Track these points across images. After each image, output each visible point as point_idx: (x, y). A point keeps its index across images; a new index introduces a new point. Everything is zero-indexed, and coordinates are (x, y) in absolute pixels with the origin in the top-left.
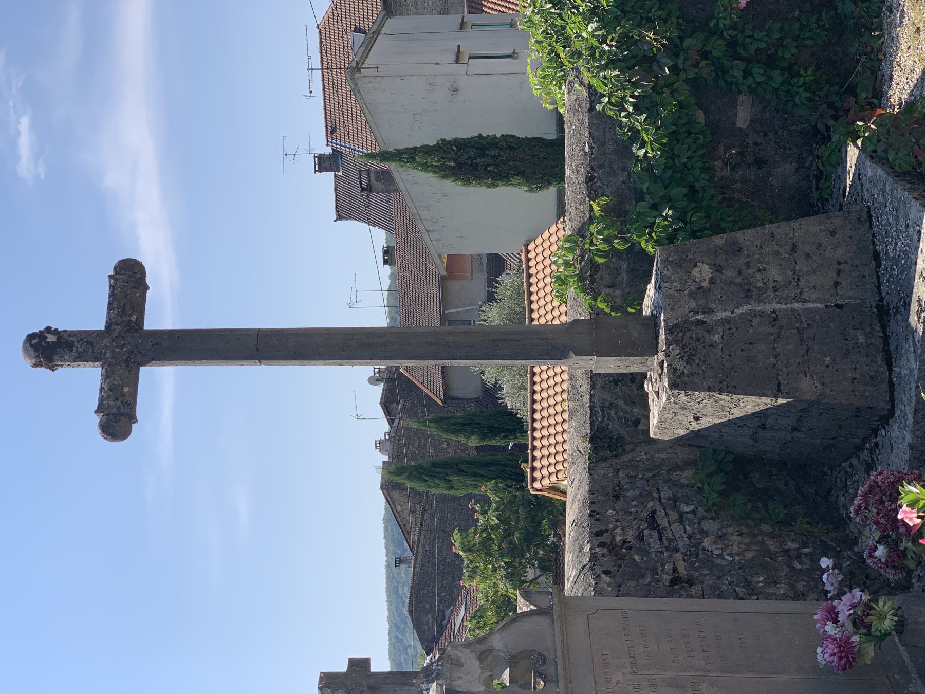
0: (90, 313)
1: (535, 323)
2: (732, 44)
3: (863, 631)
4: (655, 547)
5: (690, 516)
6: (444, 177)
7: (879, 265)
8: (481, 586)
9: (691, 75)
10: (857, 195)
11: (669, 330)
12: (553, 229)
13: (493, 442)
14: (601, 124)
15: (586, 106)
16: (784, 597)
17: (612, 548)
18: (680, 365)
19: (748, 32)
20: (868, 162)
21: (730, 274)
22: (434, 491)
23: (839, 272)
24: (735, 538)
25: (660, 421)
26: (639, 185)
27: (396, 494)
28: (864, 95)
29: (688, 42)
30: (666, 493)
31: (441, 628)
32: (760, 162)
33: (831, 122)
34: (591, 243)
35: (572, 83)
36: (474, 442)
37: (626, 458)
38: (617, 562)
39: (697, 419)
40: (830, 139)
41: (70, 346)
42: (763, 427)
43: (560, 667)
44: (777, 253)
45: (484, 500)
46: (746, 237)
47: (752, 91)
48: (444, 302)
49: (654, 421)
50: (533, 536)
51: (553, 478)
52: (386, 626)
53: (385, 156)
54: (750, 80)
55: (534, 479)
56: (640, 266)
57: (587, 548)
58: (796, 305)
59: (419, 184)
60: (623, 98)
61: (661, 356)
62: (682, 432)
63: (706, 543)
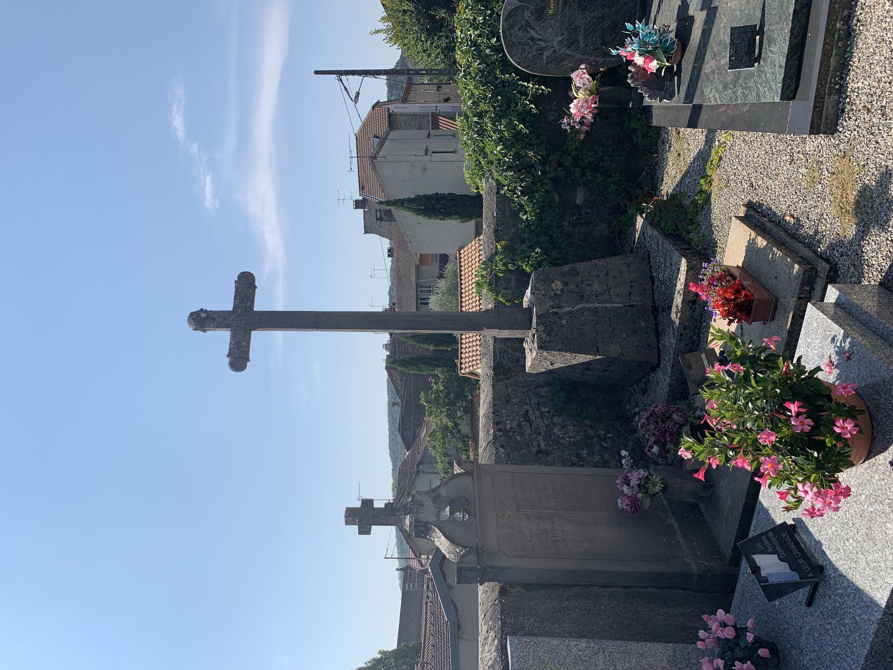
0: (225, 302)
1: (464, 309)
2: (576, 159)
3: (643, 490)
4: (528, 431)
5: (547, 414)
6: (418, 214)
7: (653, 284)
8: (434, 421)
9: (553, 176)
10: (642, 244)
11: (538, 317)
12: (473, 243)
13: (441, 348)
14: (503, 201)
15: (495, 191)
16: (596, 466)
17: (505, 432)
18: (544, 336)
19: (584, 152)
20: (649, 227)
21: (572, 287)
22: (411, 372)
23: (632, 287)
24: (571, 428)
25: (532, 364)
26: (523, 235)
27: (393, 371)
28: (646, 189)
29: (552, 157)
30: (534, 401)
31: (414, 438)
32: (588, 223)
33: (628, 203)
34: (496, 266)
35: (487, 178)
36: (431, 348)
37: (512, 380)
38: (504, 437)
39: (552, 364)
40: (627, 211)
41: (214, 319)
42: (588, 369)
43: (477, 508)
44: (598, 276)
45: (436, 377)
46: (582, 266)
47: (585, 184)
48: (418, 277)
49: (528, 364)
50: (460, 395)
51: (471, 368)
52: (388, 433)
53: (388, 203)
54: (585, 178)
55: (461, 368)
56: (522, 279)
57: (491, 432)
58: (608, 305)
59: (404, 216)
60: (515, 187)
61: (534, 331)
62: (543, 370)
63: (555, 430)
